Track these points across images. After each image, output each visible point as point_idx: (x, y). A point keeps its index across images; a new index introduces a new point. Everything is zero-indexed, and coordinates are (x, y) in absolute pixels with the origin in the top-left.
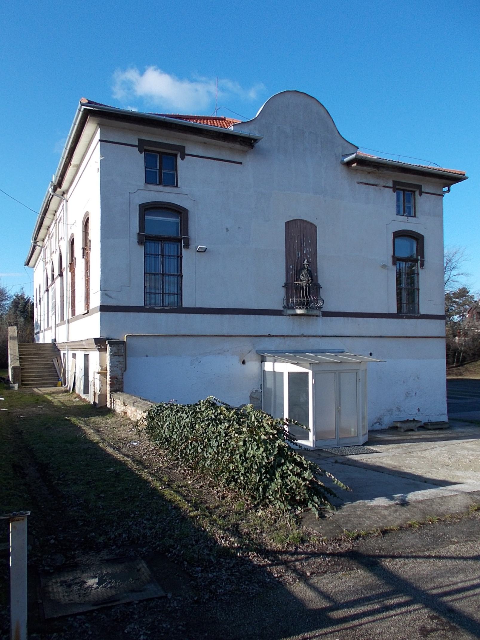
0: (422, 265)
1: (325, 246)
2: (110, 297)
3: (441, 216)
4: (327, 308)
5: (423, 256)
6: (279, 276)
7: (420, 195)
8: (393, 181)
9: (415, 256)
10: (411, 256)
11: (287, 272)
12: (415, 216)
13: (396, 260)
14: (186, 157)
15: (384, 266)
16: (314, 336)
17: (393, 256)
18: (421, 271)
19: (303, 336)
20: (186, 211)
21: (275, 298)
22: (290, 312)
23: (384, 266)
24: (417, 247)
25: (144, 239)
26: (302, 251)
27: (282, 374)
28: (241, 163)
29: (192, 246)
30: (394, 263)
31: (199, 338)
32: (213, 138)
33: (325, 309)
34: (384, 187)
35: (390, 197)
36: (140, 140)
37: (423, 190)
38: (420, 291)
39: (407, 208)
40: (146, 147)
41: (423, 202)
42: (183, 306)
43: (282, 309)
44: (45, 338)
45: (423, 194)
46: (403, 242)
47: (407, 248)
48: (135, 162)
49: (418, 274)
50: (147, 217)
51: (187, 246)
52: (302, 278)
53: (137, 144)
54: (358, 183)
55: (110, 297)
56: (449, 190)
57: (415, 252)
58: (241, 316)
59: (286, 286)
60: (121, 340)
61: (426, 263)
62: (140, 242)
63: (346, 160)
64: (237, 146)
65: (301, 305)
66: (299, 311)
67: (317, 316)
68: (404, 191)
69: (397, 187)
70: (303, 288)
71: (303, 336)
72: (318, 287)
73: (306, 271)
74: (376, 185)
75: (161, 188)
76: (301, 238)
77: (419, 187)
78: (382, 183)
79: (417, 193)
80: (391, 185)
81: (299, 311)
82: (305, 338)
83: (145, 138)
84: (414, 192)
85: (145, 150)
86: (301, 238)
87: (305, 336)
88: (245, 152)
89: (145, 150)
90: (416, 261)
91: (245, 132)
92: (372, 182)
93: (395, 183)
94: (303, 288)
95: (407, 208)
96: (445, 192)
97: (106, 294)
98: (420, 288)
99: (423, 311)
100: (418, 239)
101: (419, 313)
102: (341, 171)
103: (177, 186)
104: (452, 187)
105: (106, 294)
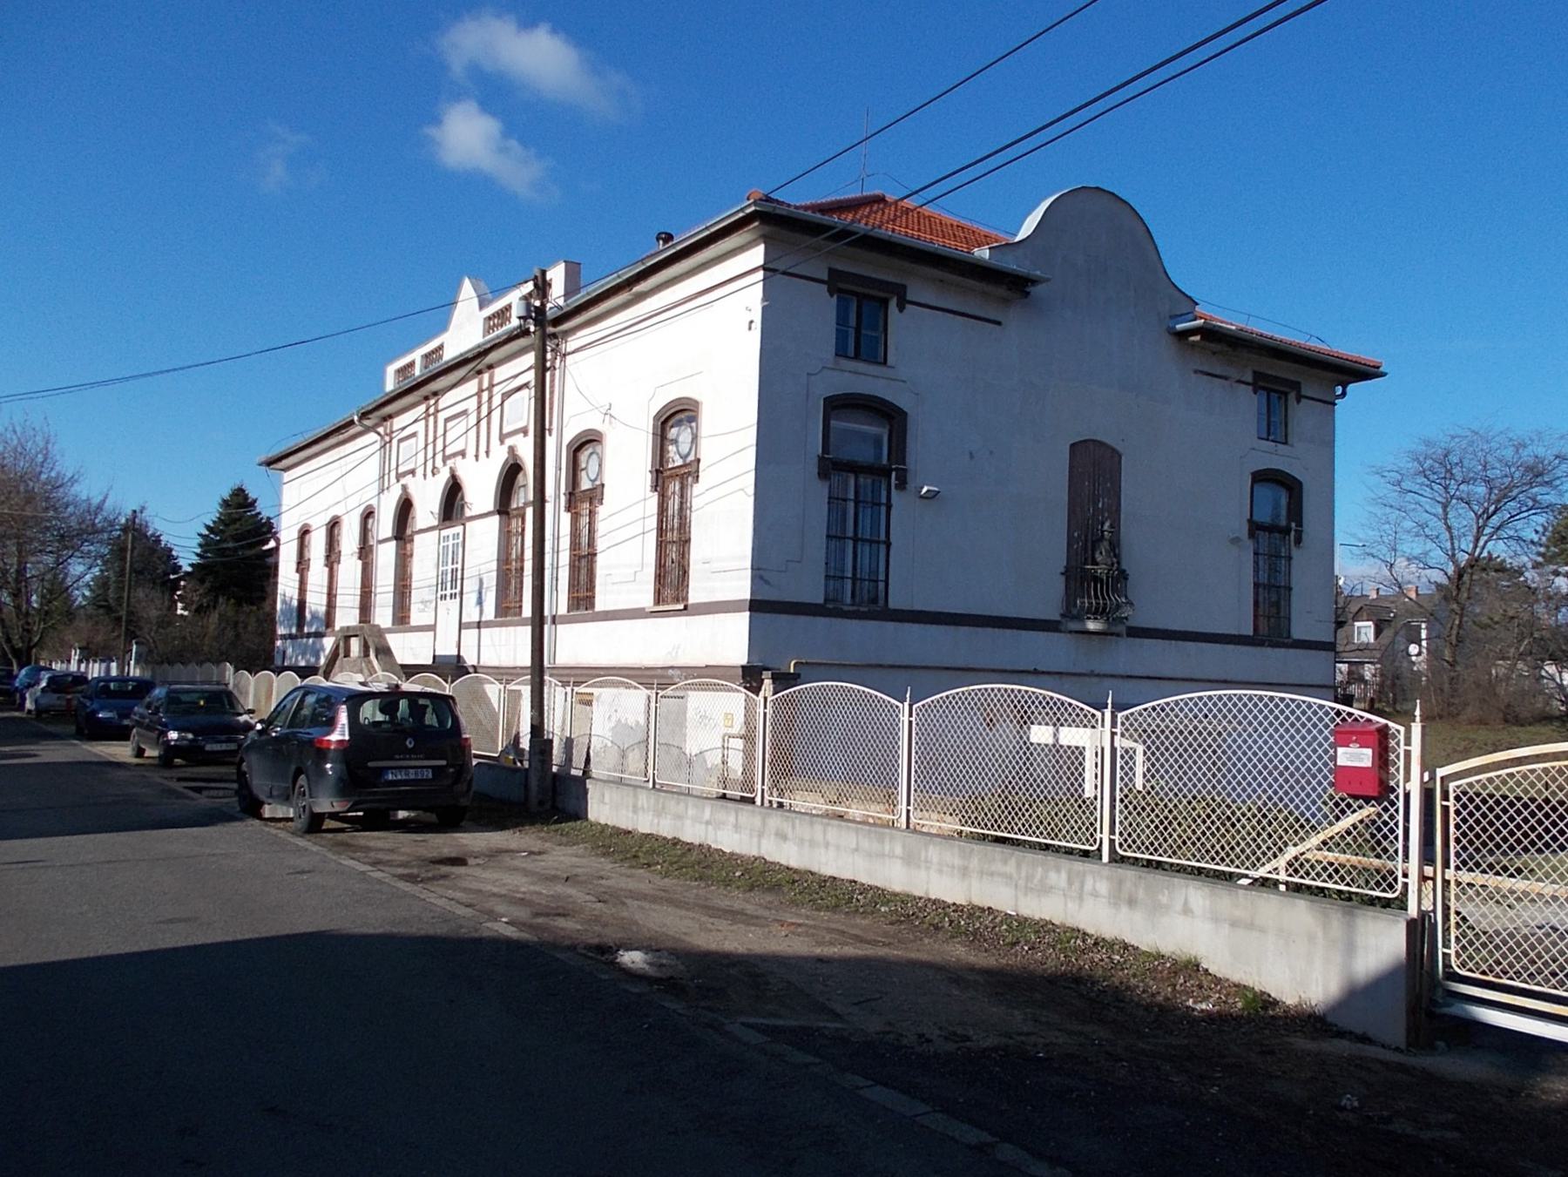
0: (1298, 541)
1: (1137, 493)
2: (767, 582)
3: (1331, 444)
4: (1140, 619)
5: (1300, 524)
6: (1055, 553)
7: (901, 308)
8: (1255, 372)
9: (1283, 523)
10: (1284, 517)
11: (1069, 545)
12: (1286, 443)
13: (1255, 528)
14: (908, 306)
15: (1236, 541)
16: (1112, 676)
17: (1250, 521)
18: (1295, 552)
19: (1092, 674)
20: (903, 414)
21: (1047, 599)
22: (1074, 626)
23: (1236, 541)
24: (1289, 504)
25: (829, 467)
26: (1095, 503)
27: (1080, 751)
28: (999, 323)
29: (911, 485)
30: (1252, 535)
31: (916, 672)
32: (963, 275)
33: (1131, 623)
34: (1239, 381)
35: (1248, 403)
36: (832, 271)
37: (1303, 392)
38: (1294, 592)
39: (1275, 429)
40: (841, 285)
41: (1302, 415)
42: (892, 605)
43: (1058, 618)
44: (430, 662)
45: (908, 306)
46: (1265, 492)
47: (1272, 503)
48: (821, 310)
49: (1290, 558)
50: (833, 423)
51: (902, 484)
52: (1099, 558)
53: (825, 278)
54: (1196, 372)
55: (767, 582)
56: (1344, 394)
57: (1284, 513)
58: (990, 630)
59: (1067, 573)
60: (784, 670)
61: (1304, 536)
62: (823, 474)
63: (1179, 327)
64: (1001, 291)
65: (1097, 613)
66: (1092, 626)
67: (1118, 635)
68: (1269, 391)
69: (1260, 383)
70: (1094, 575)
71: (1092, 674)
72: (1123, 575)
73: (1106, 543)
74: (1226, 378)
75: (861, 366)
76: (1095, 471)
77: (1296, 386)
78: (1234, 373)
79: (893, 304)
80: (1249, 379)
81: (1092, 626)
82: (1095, 680)
83: (839, 267)
84: (1286, 394)
85: (840, 291)
86: (1095, 471)
87: (1098, 675)
88: (1006, 301)
89: (840, 291)
90: (1287, 531)
91: (1011, 264)
92: (1218, 372)
93: (1257, 375)
94: (1094, 575)
95: (1275, 429)
96: (1339, 397)
97: (761, 578)
98: (1293, 585)
99: (1297, 633)
100: (1290, 486)
101: (1289, 636)
102: (1167, 347)
103: (885, 363)
104: (1351, 387)
105: (761, 578)
